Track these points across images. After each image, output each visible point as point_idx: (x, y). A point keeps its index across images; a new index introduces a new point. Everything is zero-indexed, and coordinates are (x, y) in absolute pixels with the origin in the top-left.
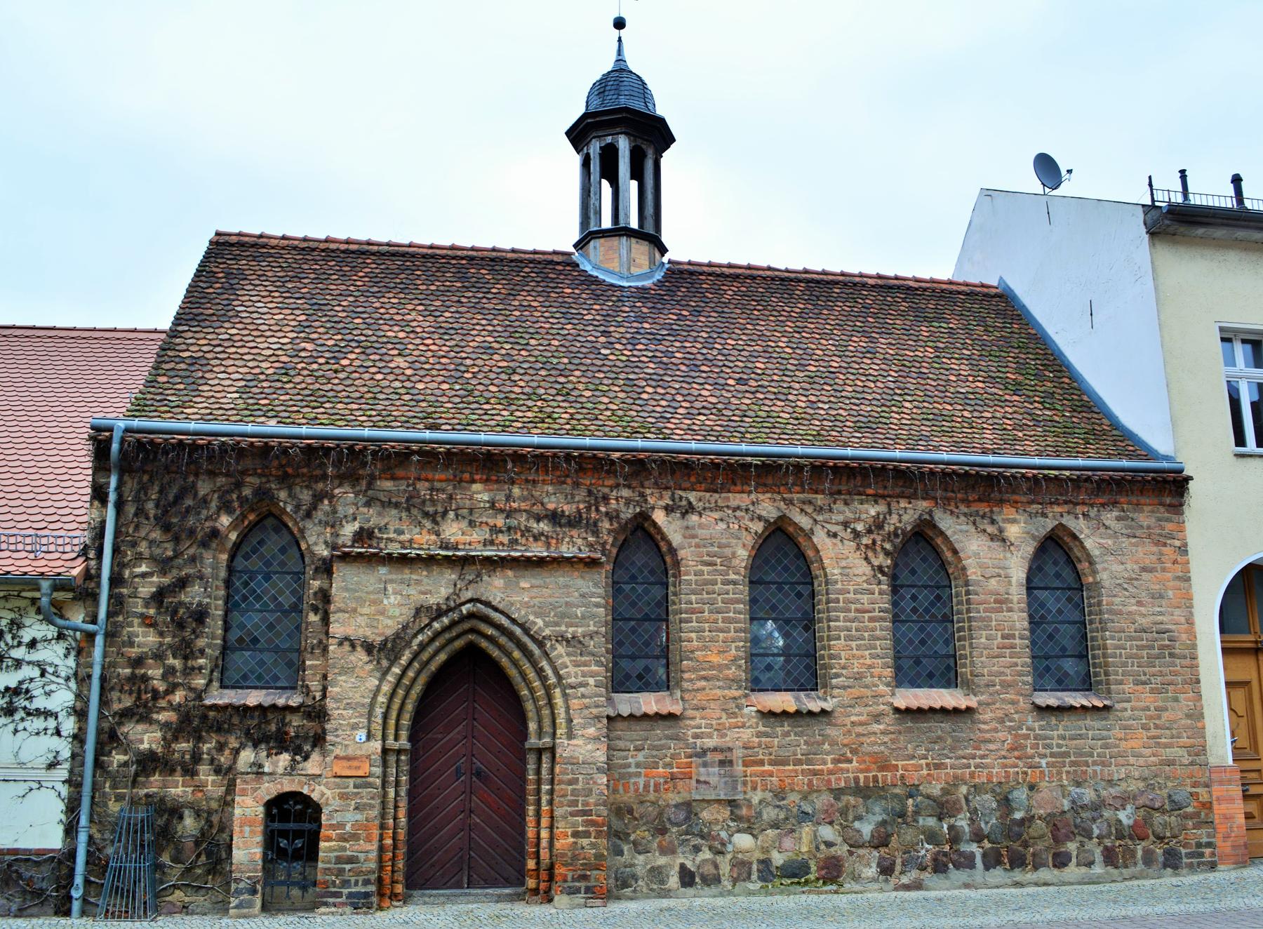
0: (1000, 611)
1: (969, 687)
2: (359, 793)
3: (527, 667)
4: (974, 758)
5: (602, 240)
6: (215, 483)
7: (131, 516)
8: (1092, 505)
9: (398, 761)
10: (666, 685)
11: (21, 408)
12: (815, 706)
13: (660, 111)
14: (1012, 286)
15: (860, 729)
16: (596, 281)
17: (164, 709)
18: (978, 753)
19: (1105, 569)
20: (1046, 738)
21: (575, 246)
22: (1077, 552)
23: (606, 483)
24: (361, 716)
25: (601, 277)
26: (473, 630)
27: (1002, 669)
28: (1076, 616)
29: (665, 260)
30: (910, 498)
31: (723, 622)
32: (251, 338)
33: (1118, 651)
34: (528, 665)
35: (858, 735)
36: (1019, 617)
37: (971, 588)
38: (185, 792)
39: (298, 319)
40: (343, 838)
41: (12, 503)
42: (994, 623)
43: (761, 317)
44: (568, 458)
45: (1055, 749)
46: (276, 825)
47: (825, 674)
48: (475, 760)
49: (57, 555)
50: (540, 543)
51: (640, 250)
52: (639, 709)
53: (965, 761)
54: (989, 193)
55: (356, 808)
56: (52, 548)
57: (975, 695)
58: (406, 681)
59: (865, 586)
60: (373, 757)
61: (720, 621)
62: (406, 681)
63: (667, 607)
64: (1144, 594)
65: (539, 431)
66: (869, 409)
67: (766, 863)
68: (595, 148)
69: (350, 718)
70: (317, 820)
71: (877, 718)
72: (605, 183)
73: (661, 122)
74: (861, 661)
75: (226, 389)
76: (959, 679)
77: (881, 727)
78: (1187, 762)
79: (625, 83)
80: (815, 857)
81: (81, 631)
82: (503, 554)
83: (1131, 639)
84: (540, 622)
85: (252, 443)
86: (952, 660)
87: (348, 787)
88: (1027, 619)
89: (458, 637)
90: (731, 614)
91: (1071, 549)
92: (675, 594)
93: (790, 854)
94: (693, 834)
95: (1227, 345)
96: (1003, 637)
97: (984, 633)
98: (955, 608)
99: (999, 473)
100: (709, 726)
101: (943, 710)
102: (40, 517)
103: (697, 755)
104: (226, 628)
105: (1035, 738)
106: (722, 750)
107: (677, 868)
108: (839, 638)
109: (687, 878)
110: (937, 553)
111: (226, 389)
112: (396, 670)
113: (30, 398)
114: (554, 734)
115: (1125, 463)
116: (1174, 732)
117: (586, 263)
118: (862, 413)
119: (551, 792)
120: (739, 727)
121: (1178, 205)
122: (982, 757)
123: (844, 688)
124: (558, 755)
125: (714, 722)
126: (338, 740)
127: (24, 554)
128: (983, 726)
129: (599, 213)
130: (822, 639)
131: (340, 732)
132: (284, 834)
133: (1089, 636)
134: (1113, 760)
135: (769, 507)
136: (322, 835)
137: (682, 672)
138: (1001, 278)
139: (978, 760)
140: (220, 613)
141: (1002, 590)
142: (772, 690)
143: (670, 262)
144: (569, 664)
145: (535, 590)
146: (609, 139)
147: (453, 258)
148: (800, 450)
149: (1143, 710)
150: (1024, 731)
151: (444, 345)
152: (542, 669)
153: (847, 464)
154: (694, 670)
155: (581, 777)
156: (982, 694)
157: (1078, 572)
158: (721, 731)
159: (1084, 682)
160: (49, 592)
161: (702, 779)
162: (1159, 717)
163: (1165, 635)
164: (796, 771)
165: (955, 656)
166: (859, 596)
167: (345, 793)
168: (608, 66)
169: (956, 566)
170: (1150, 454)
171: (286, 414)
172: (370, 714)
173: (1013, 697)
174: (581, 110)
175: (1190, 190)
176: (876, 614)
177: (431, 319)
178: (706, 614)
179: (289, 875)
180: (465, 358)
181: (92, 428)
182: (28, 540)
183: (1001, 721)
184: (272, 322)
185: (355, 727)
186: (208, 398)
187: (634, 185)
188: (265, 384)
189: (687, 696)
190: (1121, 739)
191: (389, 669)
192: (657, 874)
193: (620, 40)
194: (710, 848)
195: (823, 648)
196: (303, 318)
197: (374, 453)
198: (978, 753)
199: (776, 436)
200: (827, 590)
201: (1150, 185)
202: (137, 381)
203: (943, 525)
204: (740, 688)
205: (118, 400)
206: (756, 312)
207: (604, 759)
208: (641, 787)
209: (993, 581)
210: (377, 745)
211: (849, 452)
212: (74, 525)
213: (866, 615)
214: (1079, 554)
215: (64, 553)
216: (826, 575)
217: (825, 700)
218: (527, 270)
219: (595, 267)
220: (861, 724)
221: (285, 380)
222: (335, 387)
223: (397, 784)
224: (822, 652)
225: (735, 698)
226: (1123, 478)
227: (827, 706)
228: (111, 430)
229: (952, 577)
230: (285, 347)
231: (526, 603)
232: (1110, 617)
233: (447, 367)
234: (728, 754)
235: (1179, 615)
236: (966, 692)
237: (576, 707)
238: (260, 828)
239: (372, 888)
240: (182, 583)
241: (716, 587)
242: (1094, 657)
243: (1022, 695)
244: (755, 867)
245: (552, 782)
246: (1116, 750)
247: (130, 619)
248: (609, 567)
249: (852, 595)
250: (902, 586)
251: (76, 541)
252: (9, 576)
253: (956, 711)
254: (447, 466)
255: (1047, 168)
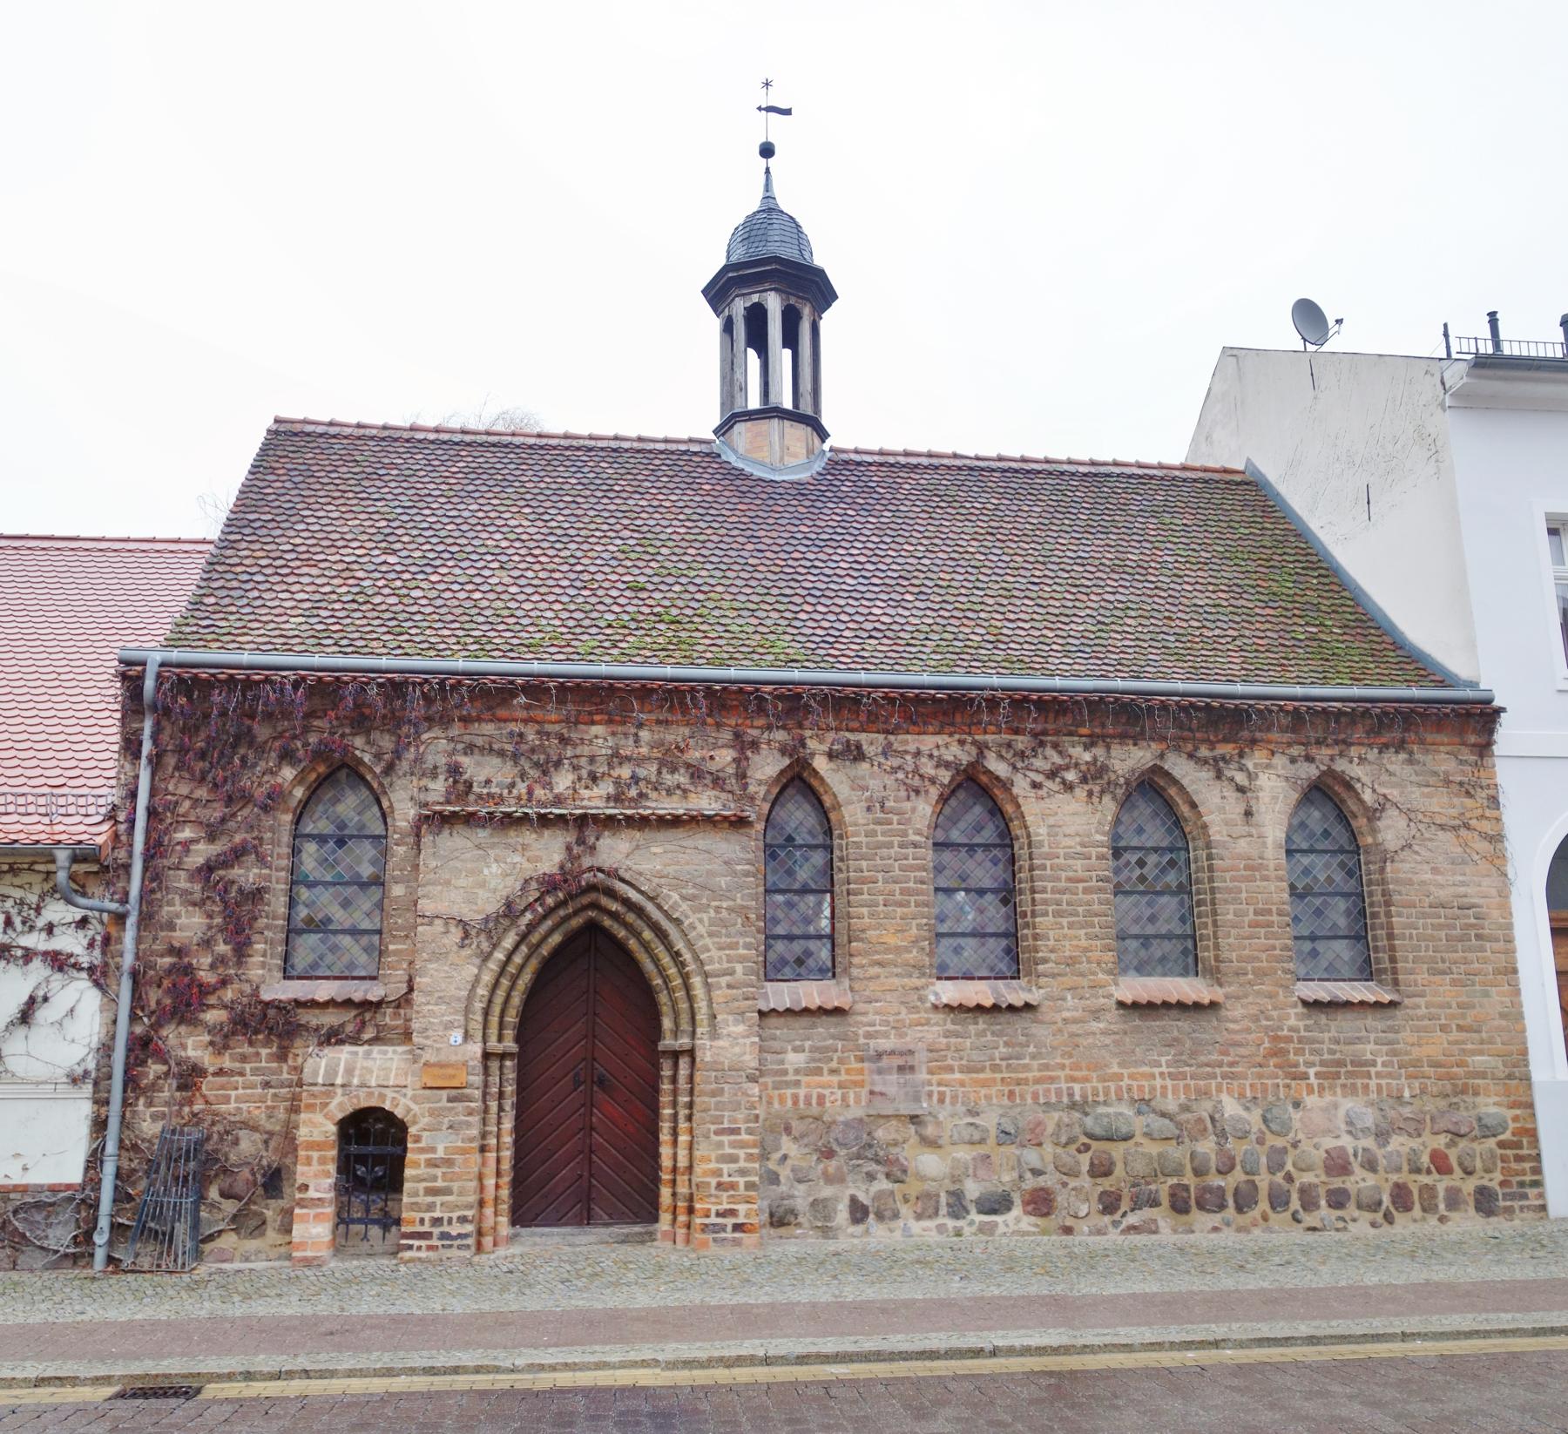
0: (1251, 879)
1: (1215, 975)
2: (453, 1108)
3: (660, 950)
4: (1220, 1066)
5: (749, 424)
6: (275, 727)
7: (170, 769)
8: (1370, 746)
9: (501, 1068)
10: (831, 971)
11: (36, 636)
12: (1017, 999)
13: (818, 261)
14: (1263, 470)
15: (1074, 1028)
16: (741, 475)
17: (213, 1007)
18: (1226, 1059)
19: (1389, 827)
20: (1313, 1041)
21: (715, 432)
22: (1352, 805)
23: (755, 724)
24: (456, 1012)
25: (748, 470)
26: (594, 906)
27: (1256, 953)
28: (1351, 885)
29: (826, 447)
30: (1136, 740)
31: (901, 894)
32: (319, 549)
33: (1407, 932)
34: (661, 948)
35: (1072, 1035)
36: (1276, 887)
37: (1214, 851)
38: (239, 1109)
39: (377, 525)
40: (432, 1164)
41: (22, 755)
42: (1244, 895)
43: (945, 516)
44: (709, 692)
45: (1326, 1056)
46: (353, 1148)
47: (1029, 959)
48: (597, 1066)
49: (78, 819)
50: (675, 798)
51: (798, 434)
52: (799, 1002)
53: (1208, 1069)
54: (1235, 352)
55: (451, 1127)
56: (72, 810)
57: (1221, 985)
58: (511, 969)
59: (1079, 849)
60: (471, 1063)
61: (898, 892)
62: (511, 969)
63: (832, 875)
64: (1440, 858)
65: (673, 661)
66: (1081, 628)
67: (957, 1196)
68: (739, 307)
69: (443, 1015)
70: (402, 1142)
71: (1096, 1014)
72: (752, 353)
73: (821, 273)
74: (1074, 943)
75: (289, 612)
76: (1200, 965)
77: (1102, 1025)
78: (1503, 1076)
79: (775, 226)
80: (1019, 1188)
81: (109, 912)
82: (629, 812)
83: (1425, 916)
84: (675, 896)
85: (320, 678)
86: (1189, 944)
87: (440, 1101)
88: (1288, 890)
89: (576, 913)
90: (911, 885)
91: (1343, 801)
92: (841, 859)
93: (988, 1184)
94: (866, 1158)
95: (1555, 538)
96: (1256, 913)
97: (1232, 907)
98: (1193, 876)
99: (1250, 706)
100: (887, 1023)
101: (1181, 1006)
102: (58, 772)
103: (871, 1059)
104: (292, 903)
105: (1300, 1042)
106: (902, 1054)
107: (846, 1201)
108: (1046, 914)
109: (859, 1212)
110: (1169, 806)
111: (289, 612)
112: (500, 955)
113: (49, 631)
114: (694, 1033)
115: (1415, 692)
116: (1484, 1035)
117: (730, 452)
118: (1072, 633)
119: (690, 1105)
120: (922, 1025)
121: (1488, 356)
122: (1231, 1064)
123: (1054, 976)
124: (698, 1060)
125: (891, 1019)
126: (428, 1042)
127: (36, 818)
128: (1231, 1026)
129: (744, 389)
130: (1024, 915)
131: (430, 1033)
132: (362, 1159)
133: (1368, 911)
134: (1403, 1071)
135: (956, 751)
136: (407, 1160)
137: (851, 955)
138: (1248, 460)
139: (1226, 1069)
140: (283, 886)
141: (1255, 854)
142: (963, 978)
143: (831, 450)
144: (711, 946)
145: (669, 856)
146: (755, 298)
147: (567, 449)
148: (995, 681)
149: (1441, 1006)
150: (1285, 1032)
151: (557, 556)
152: (678, 954)
153: (1055, 698)
154: (866, 953)
155: (726, 1087)
156: (1230, 984)
157: (1352, 831)
158: (899, 1028)
159: (1361, 970)
160: (67, 864)
161: (877, 1089)
162: (1463, 1016)
163: (1470, 912)
164: (994, 1080)
165: (1194, 937)
166: (1070, 862)
167: (435, 1109)
168: (755, 205)
169: (1195, 823)
170: (1445, 680)
171: (362, 643)
172: (467, 1011)
173: (1270, 988)
174: (721, 262)
175: (1502, 336)
176: (1094, 883)
177: (540, 524)
178: (880, 884)
179: (368, 1211)
180: (582, 572)
181: (121, 662)
182: (42, 801)
183: (1256, 1019)
184: (346, 529)
185: (449, 1026)
186: (266, 623)
187: (787, 353)
188: (337, 606)
189: (856, 986)
190: (1413, 1045)
191: (490, 954)
192: (821, 1207)
193: (767, 171)
194: (888, 1176)
195: (1027, 925)
196: (384, 523)
197: (471, 689)
198: (1226, 1059)
199: (966, 664)
200: (1030, 854)
201: (1446, 335)
202: (179, 603)
203: (1177, 773)
204: (924, 975)
205: (158, 626)
206: (938, 510)
207: (755, 1064)
208: (802, 1098)
209: (1242, 843)
210: (476, 1049)
211: (1058, 682)
212: (101, 781)
213: (1081, 886)
214: (1354, 808)
215: (87, 815)
216: (1029, 836)
217: (1030, 990)
218: (657, 462)
219: (741, 457)
220: (1075, 1021)
221: (361, 600)
222: (422, 610)
223: (501, 1095)
224: (1025, 931)
225: (917, 989)
226: (1412, 710)
227: (1033, 997)
228: (143, 664)
229: (1189, 837)
230: (361, 560)
231: (658, 872)
232: (1397, 888)
233: (560, 583)
234: (909, 1058)
235: (1489, 885)
236: (1209, 982)
237: (721, 1000)
238: (334, 1153)
239: (469, 1228)
240: (237, 854)
241: (892, 851)
242: (1375, 938)
243: (1282, 986)
244: (943, 1199)
245: (691, 1092)
246: (1406, 1058)
247: (170, 896)
248: (760, 826)
249: (1061, 861)
250: (1126, 849)
251: (101, 801)
252: (16, 845)
253: (1197, 1006)
254: (561, 702)
255: (1309, 316)
